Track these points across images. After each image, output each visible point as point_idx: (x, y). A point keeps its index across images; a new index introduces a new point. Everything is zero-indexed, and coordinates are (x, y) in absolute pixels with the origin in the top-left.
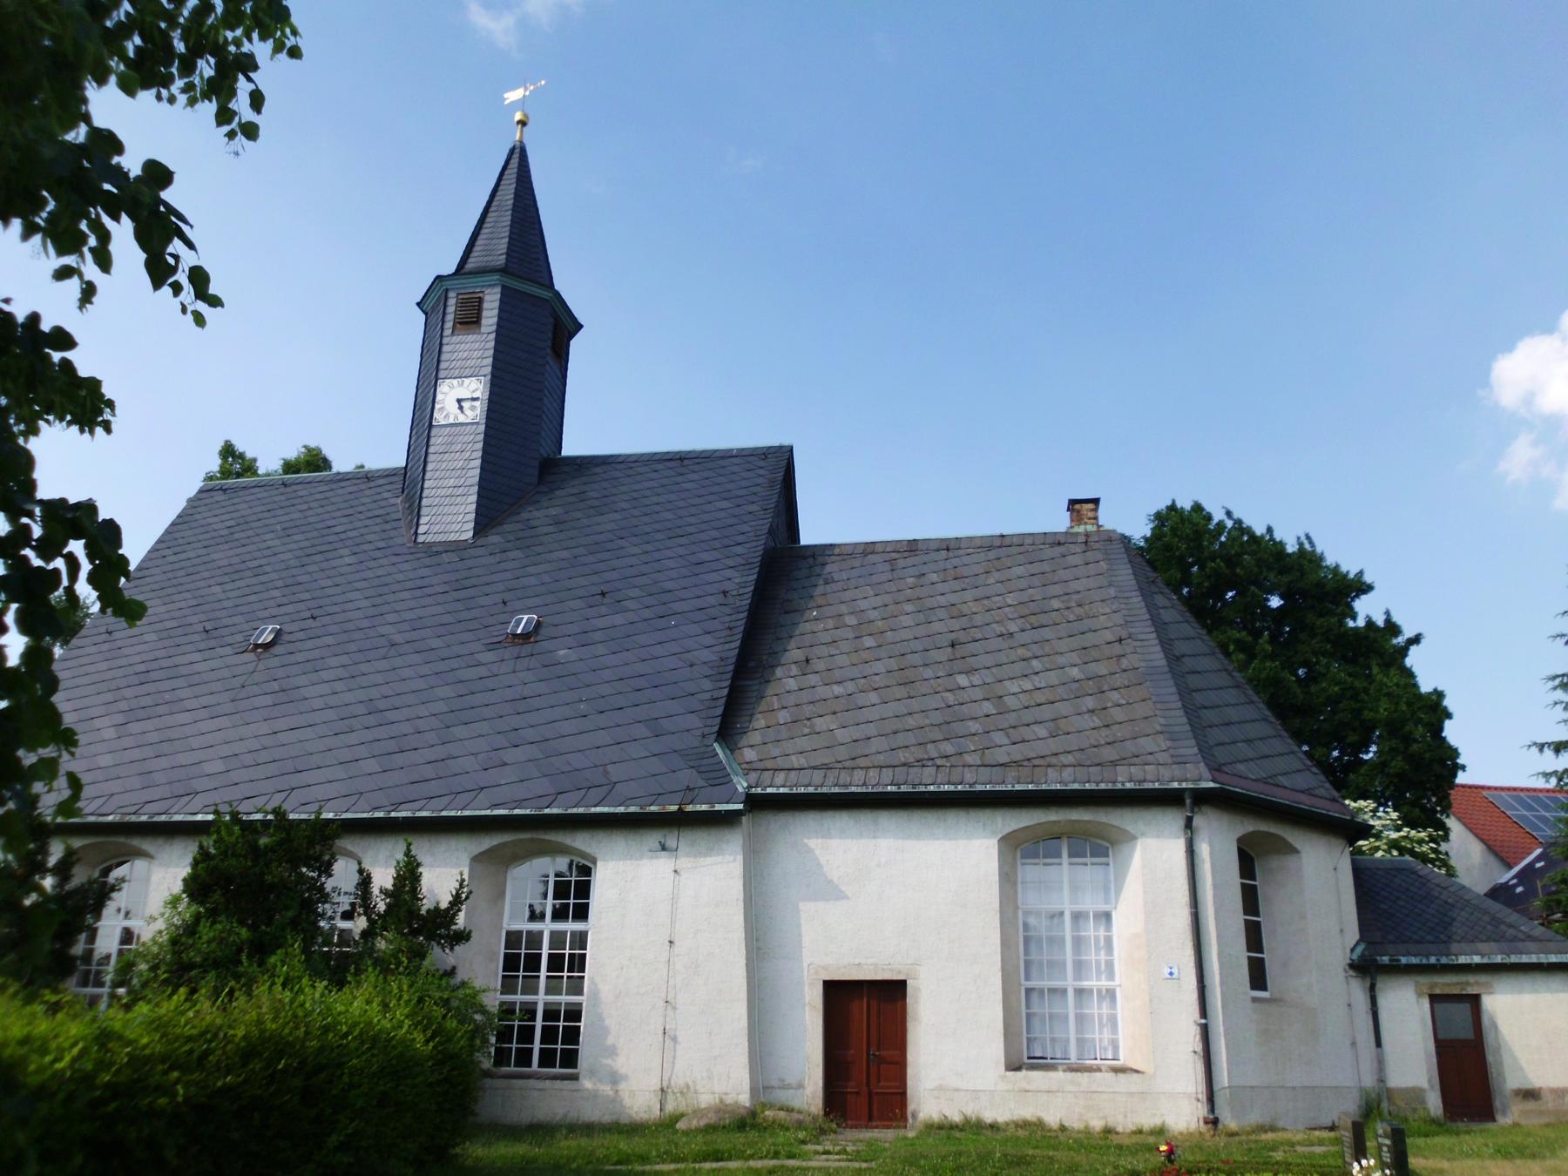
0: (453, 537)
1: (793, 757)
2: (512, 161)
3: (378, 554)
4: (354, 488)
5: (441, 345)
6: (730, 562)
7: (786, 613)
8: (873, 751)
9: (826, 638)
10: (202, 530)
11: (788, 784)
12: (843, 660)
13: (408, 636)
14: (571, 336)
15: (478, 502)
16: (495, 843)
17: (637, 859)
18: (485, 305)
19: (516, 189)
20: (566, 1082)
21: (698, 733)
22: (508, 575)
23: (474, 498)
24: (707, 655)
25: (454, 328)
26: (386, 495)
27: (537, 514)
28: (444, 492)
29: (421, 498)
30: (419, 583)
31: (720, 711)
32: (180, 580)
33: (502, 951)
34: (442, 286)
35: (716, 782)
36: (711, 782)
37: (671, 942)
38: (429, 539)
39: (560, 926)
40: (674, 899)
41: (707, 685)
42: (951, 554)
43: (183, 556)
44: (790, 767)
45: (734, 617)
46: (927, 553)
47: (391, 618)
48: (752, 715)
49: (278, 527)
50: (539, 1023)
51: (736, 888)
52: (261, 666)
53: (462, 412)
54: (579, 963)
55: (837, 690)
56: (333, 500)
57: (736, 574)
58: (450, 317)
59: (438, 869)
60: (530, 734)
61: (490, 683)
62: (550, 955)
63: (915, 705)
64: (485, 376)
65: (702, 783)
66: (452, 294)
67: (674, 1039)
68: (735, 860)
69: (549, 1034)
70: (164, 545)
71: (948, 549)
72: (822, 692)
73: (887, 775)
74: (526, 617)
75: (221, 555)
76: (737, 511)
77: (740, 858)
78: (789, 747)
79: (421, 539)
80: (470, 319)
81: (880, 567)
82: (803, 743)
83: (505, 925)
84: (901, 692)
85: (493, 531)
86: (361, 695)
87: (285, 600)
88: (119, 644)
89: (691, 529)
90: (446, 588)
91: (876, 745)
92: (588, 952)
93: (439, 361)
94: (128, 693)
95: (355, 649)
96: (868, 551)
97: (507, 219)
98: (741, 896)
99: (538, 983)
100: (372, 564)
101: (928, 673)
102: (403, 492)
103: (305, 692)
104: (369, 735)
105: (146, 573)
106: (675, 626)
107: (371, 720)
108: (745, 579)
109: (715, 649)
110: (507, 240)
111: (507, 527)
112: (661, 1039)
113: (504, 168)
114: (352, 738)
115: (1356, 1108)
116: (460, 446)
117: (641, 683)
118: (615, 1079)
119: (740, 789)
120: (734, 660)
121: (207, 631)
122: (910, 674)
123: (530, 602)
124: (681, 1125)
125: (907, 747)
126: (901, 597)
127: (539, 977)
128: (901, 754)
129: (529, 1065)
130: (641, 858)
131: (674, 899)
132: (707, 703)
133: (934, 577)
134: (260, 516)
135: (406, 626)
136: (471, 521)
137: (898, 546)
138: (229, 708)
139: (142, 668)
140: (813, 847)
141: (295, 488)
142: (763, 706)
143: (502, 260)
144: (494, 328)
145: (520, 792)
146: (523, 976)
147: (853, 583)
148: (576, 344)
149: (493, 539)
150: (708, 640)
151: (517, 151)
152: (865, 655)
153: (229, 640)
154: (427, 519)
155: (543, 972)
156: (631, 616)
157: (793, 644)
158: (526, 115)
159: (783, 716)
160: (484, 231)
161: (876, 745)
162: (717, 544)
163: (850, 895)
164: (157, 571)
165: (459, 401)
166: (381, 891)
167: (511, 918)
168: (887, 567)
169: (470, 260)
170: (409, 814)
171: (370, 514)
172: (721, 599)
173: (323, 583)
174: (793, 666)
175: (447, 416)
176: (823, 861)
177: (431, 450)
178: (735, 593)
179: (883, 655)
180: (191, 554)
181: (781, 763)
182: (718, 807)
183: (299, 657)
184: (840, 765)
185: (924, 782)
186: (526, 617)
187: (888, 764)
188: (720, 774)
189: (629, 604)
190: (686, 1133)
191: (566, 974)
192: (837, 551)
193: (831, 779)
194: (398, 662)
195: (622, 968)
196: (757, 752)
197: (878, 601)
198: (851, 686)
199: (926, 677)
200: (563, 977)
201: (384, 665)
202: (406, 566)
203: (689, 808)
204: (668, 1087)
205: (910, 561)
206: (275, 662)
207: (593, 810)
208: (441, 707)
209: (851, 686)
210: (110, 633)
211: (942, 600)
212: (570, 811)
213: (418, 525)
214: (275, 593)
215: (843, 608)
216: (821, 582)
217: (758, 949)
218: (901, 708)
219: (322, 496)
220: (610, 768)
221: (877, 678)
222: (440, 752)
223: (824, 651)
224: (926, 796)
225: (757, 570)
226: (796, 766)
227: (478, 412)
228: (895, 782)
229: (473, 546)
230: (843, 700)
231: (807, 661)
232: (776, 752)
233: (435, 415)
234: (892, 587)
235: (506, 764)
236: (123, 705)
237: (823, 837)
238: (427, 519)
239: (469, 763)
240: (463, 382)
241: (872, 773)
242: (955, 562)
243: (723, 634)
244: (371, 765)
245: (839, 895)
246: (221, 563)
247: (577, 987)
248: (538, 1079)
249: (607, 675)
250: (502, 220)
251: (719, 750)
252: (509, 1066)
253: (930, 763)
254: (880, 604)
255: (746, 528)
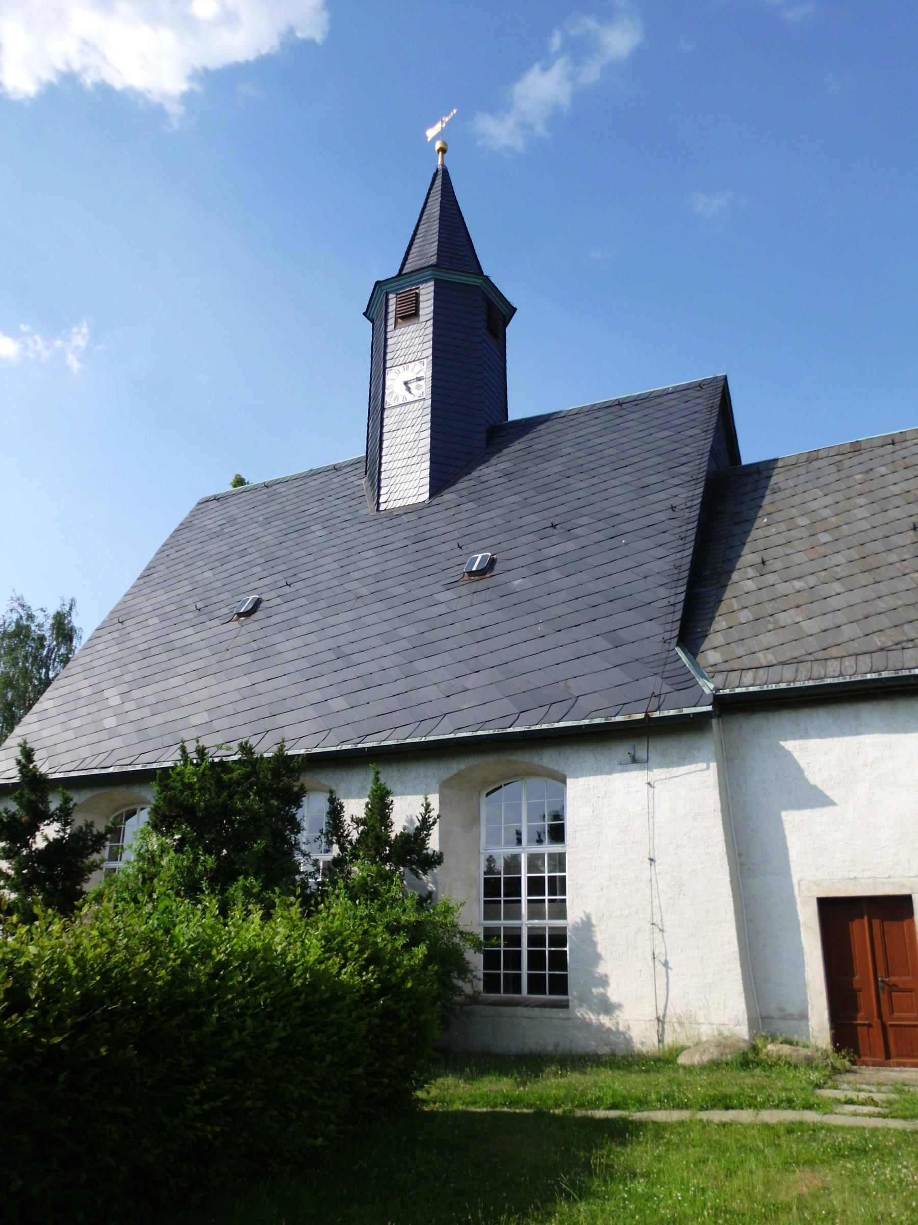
0: (411, 501)
1: (760, 655)
2: (436, 182)
3: (347, 524)
4: (326, 479)
5: (386, 339)
6: (676, 481)
7: (736, 524)
8: (845, 639)
9: (781, 539)
10: (199, 531)
11: (758, 683)
12: (801, 557)
13: (373, 588)
14: (506, 322)
15: (431, 468)
16: (463, 767)
17: (607, 774)
18: (422, 298)
19: (441, 202)
20: (555, 1010)
21: (659, 638)
22: (464, 523)
23: (428, 464)
24: (659, 566)
25: (396, 323)
26: (352, 479)
27: (486, 471)
28: (400, 464)
29: (380, 473)
30: (382, 542)
31: (679, 615)
32: (180, 572)
33: (482, 877)
34: (382, 290)
35: (681, 686)
36: (677, 687)
37: (651, 860)
38: (390, 506)
39: (537, 849)
40: (651, 814)
41: (663, 592)
42: (897, 447)
43: (184, 552)
44: (758, 665)
45: (684, 528)
46: (872, 449)
47: (356, 575)
48: (712, 618)
49: (261, 519)
50: (525, 948)
51: (712, 799)
52: (243, 631)
53: (410, 392)
54: (558, 885)
55: (798, 585)
56: (307, 491)
57: (683, 490)
58: (392, 315)
59: (409, 797)
60: (487, 660)
61: (449, 619)
62: (529, 878)
63: (883, 588)
64: (427, 357)
65: (669, 689)
66: (391, 296)
67: (666, 964)
68: (708, 768)
69: (536, 960)
70: (168, 547)
71: (893, 444)
72: (782, 588)
73: (865, 662)
74: (480, 556)
75: (214, 546)
76: (677, 437)
77: (713, 765)
78: (752, 644)
79: (382, 507)
80: (410, 314)
81: (827, 470)
82: (768, 639)
83: (482, 851)
84: (867, 578)
85: (447, 491)
86: (331, 643)
87: (265, 574)
88: (128, 630)
89: (634, 460)
90: (406, 542)
91: (848, 632)
92: (567, 874)
93: (385, 354)
94: (132, 667)
95: (325, 605)
96: (812, 458)
97: (436, 227)
98: (718, 805)
99: (520, 908)
100: (341, 533)
101: (893, 557)
102: (366, 474)
103: (279, 648)
104: (339, 677)
105: (153, 570)
106: (626, 544)
107: (340, 663)
108: (691, 493)
109: (668, 559)
110: (437, 243)
111: (459, 486)
112: (651, 964)
113: (431, 189)
114: (323, 682)
115: (681, 1044)
116: (410, 422)
117: (597, 599)
118: (607, 1007)
119: (707, 691)
120: (688, 566)
121: (199, 610)
122: (872, 561)
123: (482, 544)
124: (683, 1060)
125: (881, 631)
126: (852, 492)
127: (520, 901)
128: (876, 639)
129: (518, 990)
130: (611, 772)
131: (651, 814)
132: (665, 610)
133: (883, 470)
134: (246, 513)
135: (370, 580)
136: (426, 485)
137: (841, 449)
138: (217, 668)
139: (146, 646)
140: (790, 750)
141: (275, 487)
142: (723, 608)
143: (434, 260)
144: (432, 315)
145: (483, 714)
146: (505, 901)
147: (800, 489)
148: (512, 331)
149: (448, 497)
150: (660, 552)
151: (440, 172)
152: (822, 550)
153: (217, 614)
154: (387, 489)
155: (524, 897)
156: (583, 542)
157: (746, 549)
158: (444, 143)
159: (744, 616)
160: (416, 241)
161: (848, 632)
162: (661, 468)
163: (835, 799)
164: (163, 567)
165: (406, 383)
166: (352, 820)
167: (487, 842)
168: (833, 469)
169: (406, 266)
170: (375, 744)
171: (338, 496)
172: (670, 513)
173: (297, 555)
174: (750, 570)
175: (396, 398)
176: (802, 763)
177: (384, 430)
178: (683, 506)
179: (842, 547)
180: (188, 550)
181: (746, 662)
182: (686, 711)
183: (275, 619)
184: (811, 657)
185: (906, 666)
186: (480, 556)
187: (864, 651)
188: (687, 677)
189: (578, 531)
190: (689, 1069)
191: (547, 897)
192: (780, 464)
193: (803, 674)
194: (363, 611)
195: (602, 890)
196: (722, 654)
197: (829, 500)
198: (812, 580)
199: (890, 562)
200: (543, 901)
201: (351, 615)
202: (372, 530)
203: (656, 715)
204: (664, 1015)
205: (855, 461)
206: (256, 626)
207: (557, 725)
208: (405, 644)
209: (812, 580)
210: (122, 622)
211: (896, 489)
212: (533, 728)
213: (379, 496)
214: (258, 569)
215: (794, 512)
216: (768, 492)
217: (742, 864)
218: (869, 593)
219: (298, 489)
220: (571, 682)
221: (838, 569)
222: (401, 686)
223: (779, 551)
224: (912, 681)
225: (703, 483)
226: (764, 664)
227: (424, 390)
228: (874, 669)
229: (429, 506)
230: (805, 594)
231: (763, 562)
232: (741, 651)
233: (386, 399)
234: (842, 485)
235: (468, 690)
236: (128, 677)
237: (801, 738)
238: (387, 489)
239: (433, 692)
240: (408, 367)
241: (848, 662)
242: (904, 453)
243: (675, 544)
244: (339, 704)
245: (826, 802)
246: (212, 553)
247: (560, 910)
248: (526, 1006)
249: (562, 596)
250: (432, 228)
251: (681, 654)
252: (499, 992)
253: (910, 645)
254: (832, 502)
255: (688, 450)
